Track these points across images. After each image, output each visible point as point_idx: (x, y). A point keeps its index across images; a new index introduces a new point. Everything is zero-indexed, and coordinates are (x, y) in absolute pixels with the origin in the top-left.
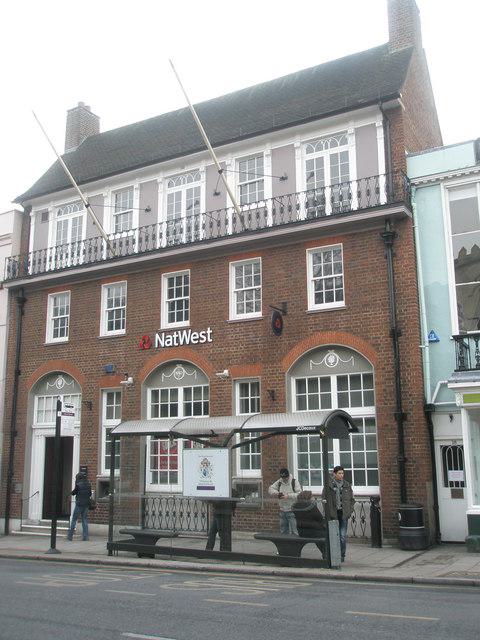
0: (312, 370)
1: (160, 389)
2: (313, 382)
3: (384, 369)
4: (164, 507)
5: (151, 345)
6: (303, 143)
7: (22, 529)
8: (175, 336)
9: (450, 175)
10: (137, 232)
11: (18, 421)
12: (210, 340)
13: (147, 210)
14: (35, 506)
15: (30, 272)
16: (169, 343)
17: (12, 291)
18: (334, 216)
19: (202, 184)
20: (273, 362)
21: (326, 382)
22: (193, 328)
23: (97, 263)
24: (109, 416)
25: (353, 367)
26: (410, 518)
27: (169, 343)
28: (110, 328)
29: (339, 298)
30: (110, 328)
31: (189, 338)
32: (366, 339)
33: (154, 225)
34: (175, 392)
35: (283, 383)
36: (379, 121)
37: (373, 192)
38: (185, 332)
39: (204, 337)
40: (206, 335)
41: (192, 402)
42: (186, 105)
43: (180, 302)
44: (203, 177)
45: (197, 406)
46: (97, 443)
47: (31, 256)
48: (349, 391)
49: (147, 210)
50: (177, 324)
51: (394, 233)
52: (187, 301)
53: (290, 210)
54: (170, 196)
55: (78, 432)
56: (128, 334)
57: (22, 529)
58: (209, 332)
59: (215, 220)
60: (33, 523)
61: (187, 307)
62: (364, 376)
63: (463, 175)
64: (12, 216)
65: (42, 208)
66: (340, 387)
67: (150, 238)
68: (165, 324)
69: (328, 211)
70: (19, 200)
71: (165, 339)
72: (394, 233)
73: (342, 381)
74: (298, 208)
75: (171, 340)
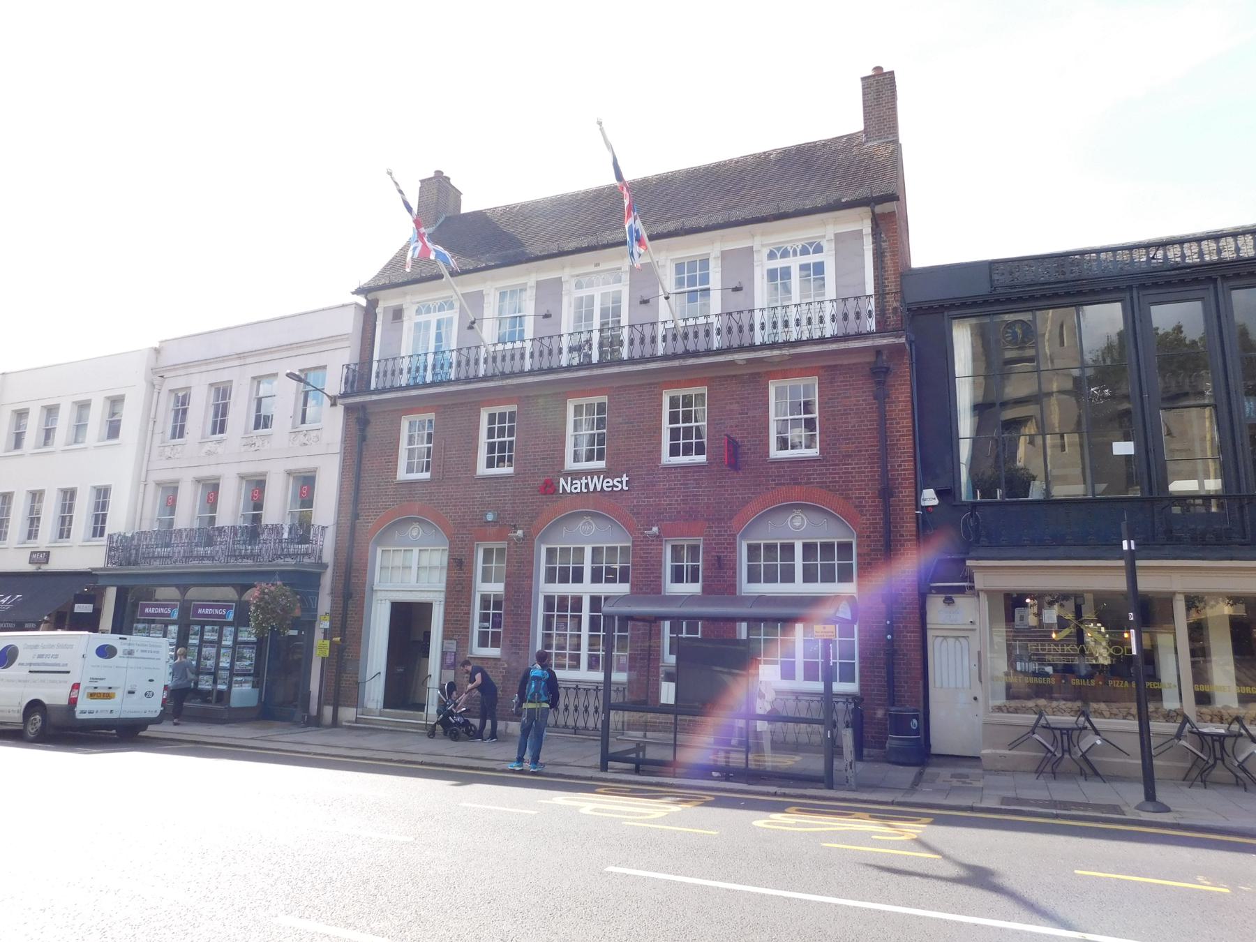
0: (770, 533)
1: (779, 542)
2: (770, 548)
3: (869, 537)
5: (556, 490)
6: (572, 276)
7: (357, 721)
8: (584, 481)
9: (1110, 286)
10: (454, 354)
11: (353, 580)
12: (626, 488)
13: (547, 316)
14: (375, 691)
15: (373, 386)
16: (576, 488)
17: (348, 409)
18: (601, 364)
19: (454, 315)
21: (788, 549)
22: (608, 473)
23: (393, 389)
24: (486, 579)
25: (830, 532)
26: (899, 724)
27: (576, 488)
28: (490, 464)
29: (600, 458)
30: (490, 464)
31: (597, 483)
32: (848, 498)
33: (653, 324)
35: (733, 547)
36: (867, 227)
37: (746, 329)
38: (596, 477)
39: (619, 485)
40: (621, 482)
41: (558, 566)
43: (502, 444)
44: (626, 278)
45: (564, 571)
46: (468, 613)
47: (375, 365)
49: (547, 316)
50: (584, 465)
51: (888, 369)
52: (511, 443)
53: (393, 374)
54: (418, 325)
55: (442, 597)
56: (516, 473)
57: (357, 721)
58: (625, 479)
59: (467, 355)
60: (370, 712)
61: (511, 450)
62: (840, 545)
63: (1044, 296)
64: (352, 311)
65: (394, 303)
66: (805, 557)
67: (472, 362)
68: (570, 465)
69: (595, 358)
70: (358, 292)
72: (888, 369)
73: (809, 549)
74: (401, 373)
75: (579, 486)
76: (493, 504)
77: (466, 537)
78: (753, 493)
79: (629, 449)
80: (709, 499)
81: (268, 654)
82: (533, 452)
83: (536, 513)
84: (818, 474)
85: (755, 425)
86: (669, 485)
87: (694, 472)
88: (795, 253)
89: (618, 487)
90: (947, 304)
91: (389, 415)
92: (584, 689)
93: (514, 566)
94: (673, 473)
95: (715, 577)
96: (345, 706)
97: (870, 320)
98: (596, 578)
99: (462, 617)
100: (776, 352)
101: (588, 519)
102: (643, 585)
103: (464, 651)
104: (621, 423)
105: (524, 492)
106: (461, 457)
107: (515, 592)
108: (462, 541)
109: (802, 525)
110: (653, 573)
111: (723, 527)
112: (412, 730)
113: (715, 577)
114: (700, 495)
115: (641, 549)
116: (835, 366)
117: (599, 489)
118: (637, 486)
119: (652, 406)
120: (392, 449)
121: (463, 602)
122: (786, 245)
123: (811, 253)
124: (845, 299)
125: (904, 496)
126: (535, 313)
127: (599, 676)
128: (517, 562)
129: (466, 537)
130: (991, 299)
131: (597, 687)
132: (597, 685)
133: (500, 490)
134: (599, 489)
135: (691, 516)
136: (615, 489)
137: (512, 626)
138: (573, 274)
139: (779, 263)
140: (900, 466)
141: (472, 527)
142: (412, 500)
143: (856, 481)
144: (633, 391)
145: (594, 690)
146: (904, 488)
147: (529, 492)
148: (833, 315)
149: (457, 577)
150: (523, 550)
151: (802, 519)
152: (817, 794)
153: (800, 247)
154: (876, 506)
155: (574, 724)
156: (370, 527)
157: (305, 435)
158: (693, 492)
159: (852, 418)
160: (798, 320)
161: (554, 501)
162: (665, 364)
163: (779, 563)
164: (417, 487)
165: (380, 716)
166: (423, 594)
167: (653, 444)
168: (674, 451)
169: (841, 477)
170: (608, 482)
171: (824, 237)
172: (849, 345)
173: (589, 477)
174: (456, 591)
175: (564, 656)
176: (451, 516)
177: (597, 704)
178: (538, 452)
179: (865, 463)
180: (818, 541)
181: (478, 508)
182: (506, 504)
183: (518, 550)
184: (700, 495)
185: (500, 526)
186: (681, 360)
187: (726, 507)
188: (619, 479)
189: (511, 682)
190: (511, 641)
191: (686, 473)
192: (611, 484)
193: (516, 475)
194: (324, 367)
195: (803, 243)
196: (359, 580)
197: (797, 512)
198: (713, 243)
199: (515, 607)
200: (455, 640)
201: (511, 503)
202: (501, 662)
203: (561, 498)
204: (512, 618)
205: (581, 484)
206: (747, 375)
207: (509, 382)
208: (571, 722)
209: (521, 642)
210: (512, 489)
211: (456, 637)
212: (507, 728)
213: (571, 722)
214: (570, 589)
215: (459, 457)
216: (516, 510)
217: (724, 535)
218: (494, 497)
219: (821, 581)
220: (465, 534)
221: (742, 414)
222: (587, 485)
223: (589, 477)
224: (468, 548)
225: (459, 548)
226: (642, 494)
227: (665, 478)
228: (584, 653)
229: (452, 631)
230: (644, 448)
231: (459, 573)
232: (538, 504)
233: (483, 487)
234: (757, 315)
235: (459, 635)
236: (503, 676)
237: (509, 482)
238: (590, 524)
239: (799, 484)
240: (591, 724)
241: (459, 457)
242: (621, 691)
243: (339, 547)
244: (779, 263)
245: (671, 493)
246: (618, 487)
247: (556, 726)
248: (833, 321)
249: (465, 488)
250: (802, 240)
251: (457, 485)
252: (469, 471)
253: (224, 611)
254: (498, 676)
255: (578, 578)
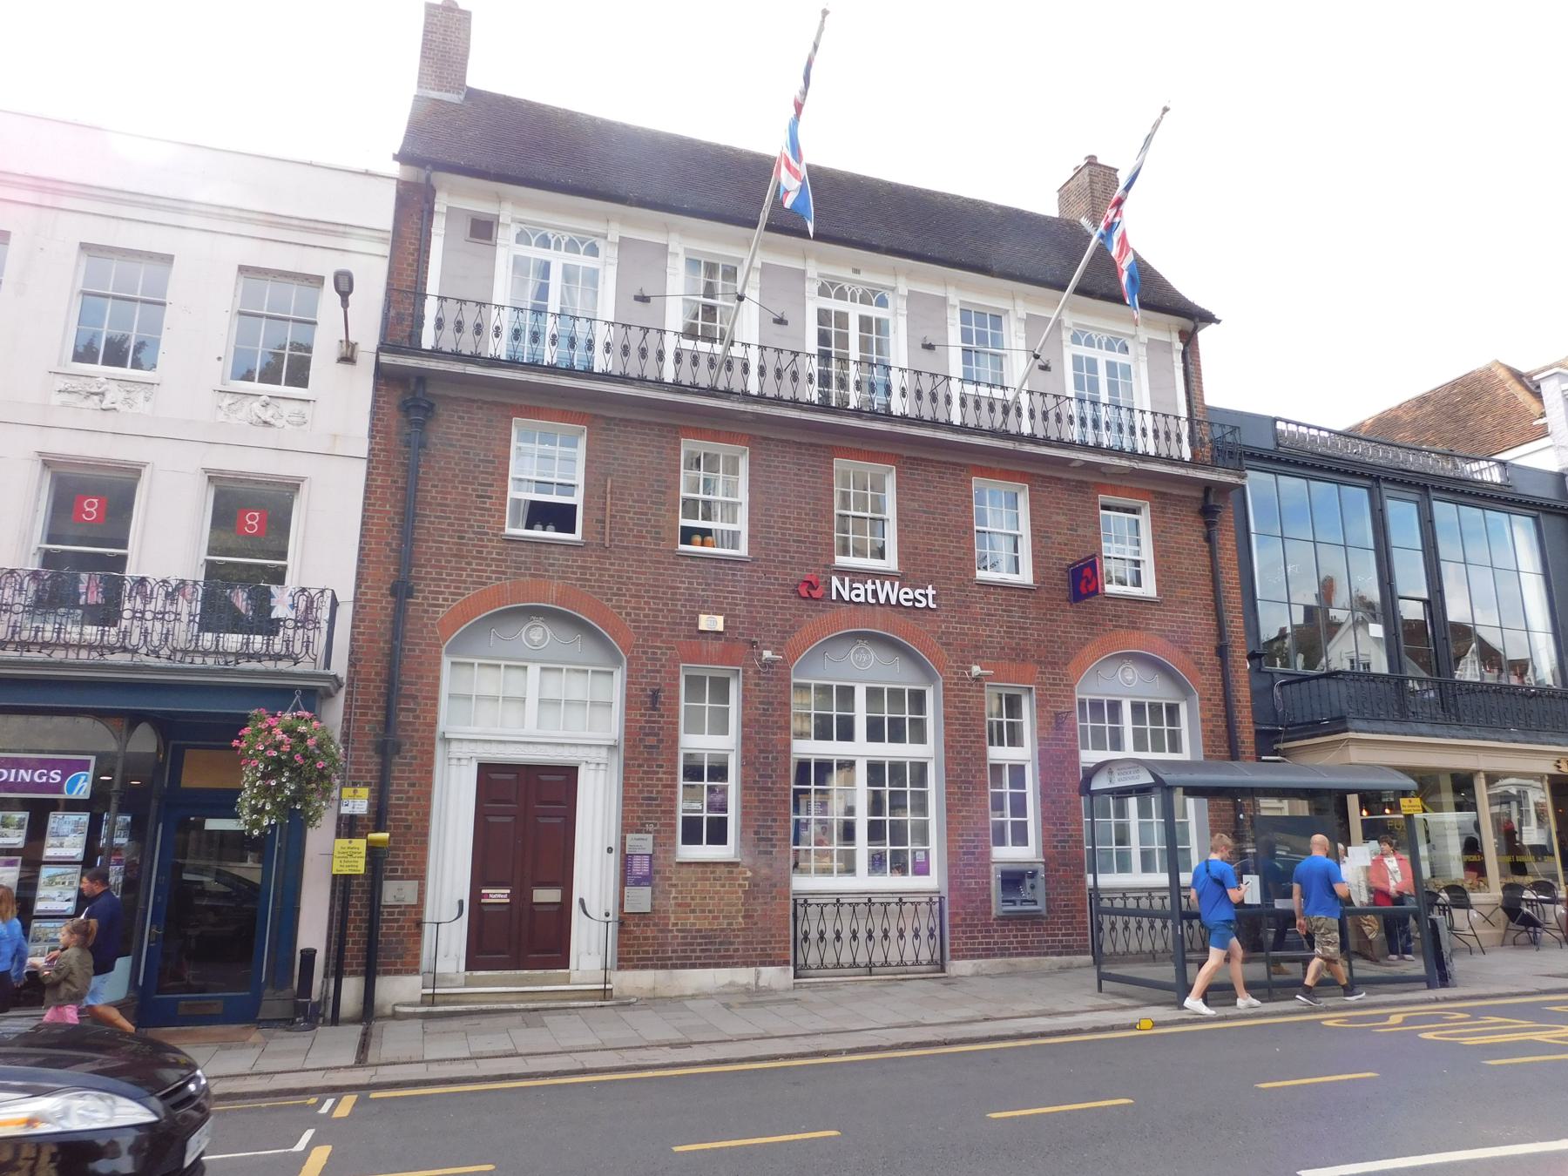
2: (824, 690)
3: (1209, 700)
4: (878, 922)
8: (870, 586)
20: (1054, 664)
21: (1115, 707)
31: (890, 592)
32: (1187, 652)
34: (847, 694)
38: (887, 584)
40: (926, 596)
42: (765, 140)
47: (431, 308)
48: (707, 704)
58: (931, 592)
60: (448, 980)
69: (428, 341)
71: (852, 589)
73: (1137, 708)
75: (862, 592)
76: (713, 602)
77: (662, 654)
78: (1089, 634)
79: (931, 550)
80: (1039, 635)
81: (154, 877)
82: (780, 528)
83: (790, 626)
84: (1157, 620)
85: (1086, 547)
86: (988, 609)
87: (1019, 596)
88: (558, 246)
89: (920, 602)
90: (1257, 453)
91: (481, 408)
92: (850, 904)
93: (757, 709)
94: (994, 594)
95: (1052, 739)
96: (387, 973)
97: (811, 386)
98: (874, 733)
99: (658, 792)
100: (1116, 461)
101: (863, 644)
102: (961, 747)
103: (666, 851)
104: (917, 511)
105: (769, 590)
106: (646, 514)
107: (761, 751)
108: (653, 659)
109: (1134, 680)
110: (973, 731)
111: (1058, 674)
112: (586, 1004)
113: (1052, 739)
114: (1028, 629)
115: (955, 696)
116: (1165, 494)
117: (893, 602)
118: (945, 605)
119: (960, 495)
120: (492, 474)
121: (661, 766)
122: (546, 230)
123: (533, 243)
124: (627, 326)
125: (1238, 657)
126: (947, 350)
127: (1161, 879)
128: (761, 703)
129: (662, 654)
130: (1275, 456)
131: (931, 899)
132: (870, 896)
133: (723, 580)
134: (893, 602)
135: (1017, 655)
136: (917, 604)
137: (756, 807)
138: (518, 216)
139: (833, 305)
140: (1232, 622)
141: (673, 636)
142: (542, 576)
143: (1194, 634)
144: (931, 469)
145: (834, 905)
146: (1236, 647)
147: (776, 590)
148: (608, 344)
149: (647, 722)
150: (772, 683)
151: (544, 630)
152: (1279, 1009)
153: (567, 239)
154: (1214, 665)
155: (868, 959)
156: (441, 615)
157: (266, 405)
158: (1019, 622)
159: (1185, 559)
160: (918, 391)
161: (820, 611)
162: (544, 378)
163: (707, 704)
164: (553, 553)
165: (466, 986)
166: (560, 750)
167: (962, 548)
168: (880, 553)
169: (1179, 627)
170: (906, 593)
171: (893, 289)
172: (468, 368)
173: (877, 582)
174: (645, 747)
175: (829, 853)
176: (628, 614)
177: (931, 924)
178: (790, 529)
179: (1200, 614)
180: (1164, 702)
181: (682, 606)
182: (737, 605)
183: (762, 682)
184: (1028, 629)
185: (727, 640)
186: (1017, 444)
187: (1060, 648)
188: (923, 592)
189: (761, 901)
190: (756, 833)
191: (1007, 595)
192: (911, 596)
193: (753, 560)
194: (168, 259)
195: (865, 287)
196: (415, 717)
197: (537, 621)
198: (668, 232)
199: (760, 776)
200: (649, 832)
201: (745, 605)
202: (740, 869)
203: (831, 607)
204: (758, 795)
205: (866, 590)
206: (1073, 481)
207: (750, 408)
208: (862, 958)
209: (774, 833)
210: (745, 582)
211: (651, 828)
212: (758, 978)
213: (862, 958)
214: (887, 751)
215: (642, 514)
216: (756, 617)
217: (1060, 685)
218: (714, 591)
219: (910, 742)
220: (659, 648)
221: (1071, 530)
222: (875, 593)
223: (877, 582)
224: (666, 672)
225: (648, 671)
226: (952, 617)
227: (982, 598)
228: (1135, 848)
229: (639, 818)
230: (952, 552)
231: (650, 716)
232: (793, 611)
233: (692, 572)
234: (894, 374)
235: (655, 825)
236: (745, 892)
237: (741, 570)
238: (867, 652)
239: (1138, 629)
240: (1159, 945)
241: (642, 514)
242: (935, 903)
243: (360, 647)
244: (833, 305)
245: (991, 620)
246: (920, 602)
247: (822, 966)
248: (608, 352)
249: (656, 568)
250: (572, 230)
251: (639, 561)
252: (663, 540)
253: (55, 775)
254: (737, 892)
255: (847, 733)
